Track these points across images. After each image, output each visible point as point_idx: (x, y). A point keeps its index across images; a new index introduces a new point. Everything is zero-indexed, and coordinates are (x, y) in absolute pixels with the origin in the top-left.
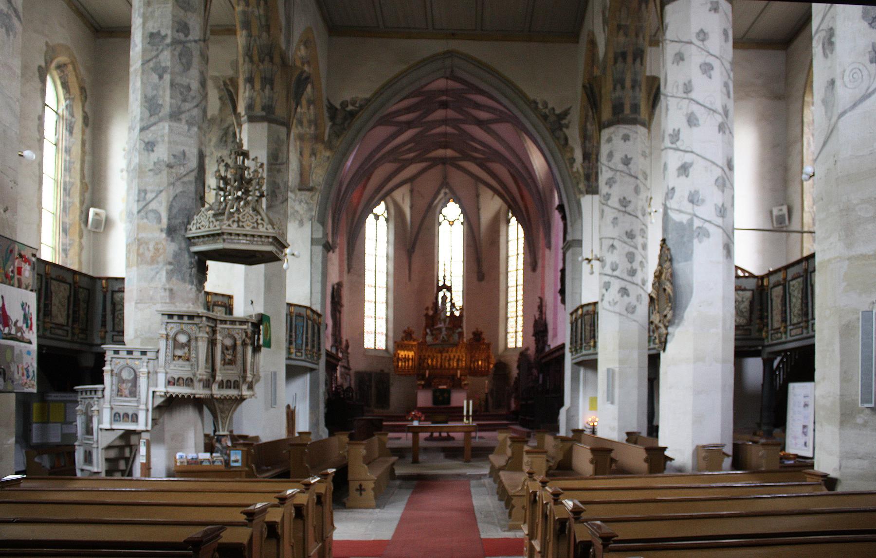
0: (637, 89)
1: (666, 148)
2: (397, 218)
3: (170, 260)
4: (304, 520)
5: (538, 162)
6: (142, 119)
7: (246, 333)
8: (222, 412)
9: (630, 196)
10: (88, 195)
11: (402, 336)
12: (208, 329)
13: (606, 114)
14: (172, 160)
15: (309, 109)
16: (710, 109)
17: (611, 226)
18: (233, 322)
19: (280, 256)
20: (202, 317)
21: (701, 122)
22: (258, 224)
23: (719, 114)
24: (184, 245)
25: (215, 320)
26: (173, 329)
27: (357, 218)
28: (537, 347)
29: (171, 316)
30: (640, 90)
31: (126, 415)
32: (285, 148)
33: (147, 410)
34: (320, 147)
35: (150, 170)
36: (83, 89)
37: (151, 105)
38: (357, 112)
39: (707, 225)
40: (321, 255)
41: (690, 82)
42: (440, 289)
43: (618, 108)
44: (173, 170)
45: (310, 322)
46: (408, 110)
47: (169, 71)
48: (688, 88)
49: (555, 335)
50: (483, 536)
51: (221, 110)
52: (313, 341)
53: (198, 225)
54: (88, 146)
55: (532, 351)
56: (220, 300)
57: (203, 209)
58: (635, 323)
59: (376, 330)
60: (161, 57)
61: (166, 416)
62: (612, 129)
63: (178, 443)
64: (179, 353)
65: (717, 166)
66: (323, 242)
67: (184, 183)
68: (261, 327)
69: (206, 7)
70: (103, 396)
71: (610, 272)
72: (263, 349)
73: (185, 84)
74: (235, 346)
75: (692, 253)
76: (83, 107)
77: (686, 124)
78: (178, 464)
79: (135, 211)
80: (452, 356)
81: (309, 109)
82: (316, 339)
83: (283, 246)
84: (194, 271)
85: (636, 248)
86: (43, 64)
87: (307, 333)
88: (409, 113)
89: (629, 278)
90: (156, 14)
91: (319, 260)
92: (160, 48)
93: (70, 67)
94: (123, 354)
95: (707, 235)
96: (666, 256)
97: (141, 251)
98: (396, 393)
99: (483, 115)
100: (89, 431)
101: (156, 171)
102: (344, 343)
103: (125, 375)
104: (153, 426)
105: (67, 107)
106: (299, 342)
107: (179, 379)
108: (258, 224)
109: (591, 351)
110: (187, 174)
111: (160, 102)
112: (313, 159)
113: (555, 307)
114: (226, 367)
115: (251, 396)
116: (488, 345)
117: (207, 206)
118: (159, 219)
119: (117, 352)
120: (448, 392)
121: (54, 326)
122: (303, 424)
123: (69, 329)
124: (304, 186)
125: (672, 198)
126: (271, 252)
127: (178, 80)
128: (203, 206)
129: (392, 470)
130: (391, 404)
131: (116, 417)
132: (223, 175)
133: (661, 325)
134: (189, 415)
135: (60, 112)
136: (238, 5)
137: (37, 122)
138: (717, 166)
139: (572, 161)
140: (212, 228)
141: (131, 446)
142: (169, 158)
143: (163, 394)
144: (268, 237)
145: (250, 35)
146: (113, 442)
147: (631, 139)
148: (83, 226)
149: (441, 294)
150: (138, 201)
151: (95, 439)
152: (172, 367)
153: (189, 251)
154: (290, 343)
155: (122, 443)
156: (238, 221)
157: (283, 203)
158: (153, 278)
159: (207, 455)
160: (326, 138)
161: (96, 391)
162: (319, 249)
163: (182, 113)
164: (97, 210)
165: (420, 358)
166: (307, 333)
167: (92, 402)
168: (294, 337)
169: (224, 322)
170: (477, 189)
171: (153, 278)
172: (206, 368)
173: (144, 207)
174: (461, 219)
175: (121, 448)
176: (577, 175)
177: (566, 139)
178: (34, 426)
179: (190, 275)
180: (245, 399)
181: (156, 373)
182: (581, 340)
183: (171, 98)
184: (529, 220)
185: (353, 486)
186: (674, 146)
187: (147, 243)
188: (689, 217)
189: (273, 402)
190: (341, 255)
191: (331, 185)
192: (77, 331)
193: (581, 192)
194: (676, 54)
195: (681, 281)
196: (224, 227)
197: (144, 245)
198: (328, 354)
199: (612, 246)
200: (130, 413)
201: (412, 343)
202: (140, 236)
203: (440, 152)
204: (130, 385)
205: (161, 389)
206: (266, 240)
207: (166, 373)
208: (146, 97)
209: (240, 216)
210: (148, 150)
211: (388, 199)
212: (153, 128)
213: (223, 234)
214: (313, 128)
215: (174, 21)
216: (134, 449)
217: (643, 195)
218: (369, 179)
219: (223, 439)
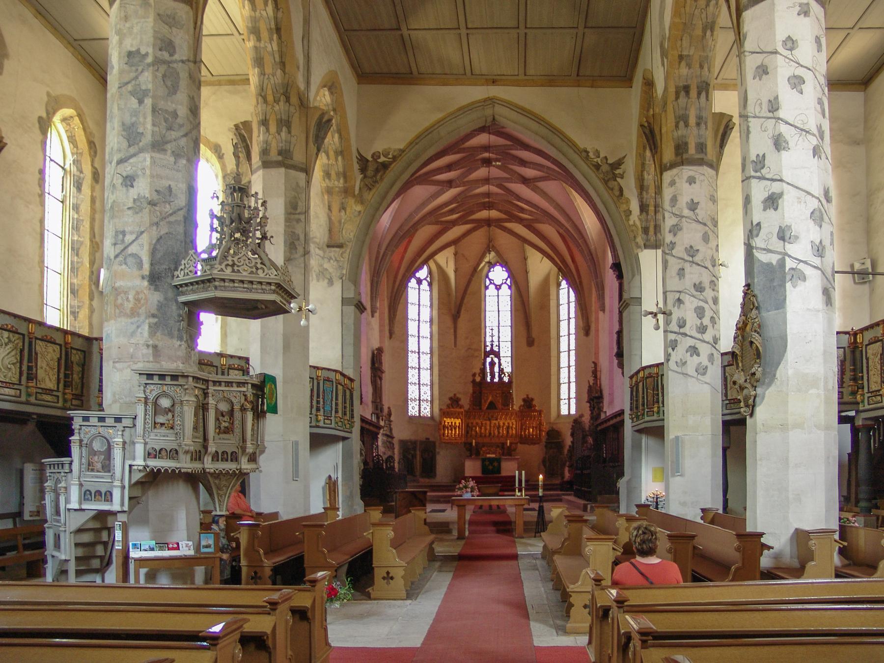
0: (703, 126)
1: (750, 177)
2: (439, 280)
3: (154, 311)
4: (270, 653)
5: (589, 221)
7: (245, 396)
8: (219, 488)
9: (699, 245)
11: (450, 404)
13: (668, 154)
14: (155, 197)
15: (337, 160)
16: (802, 130)
17: (677, 278)
20: (187, 376)
21: (791, 144)
22: (257, 269)
23: (814, 135)
24: (170, 294)
25: (207, 381)
26: (153, 391)
27: (397, 283)
28: (592, 413)
29: (150, 376)
30: (706, 128)
31: (99, 493)
33: (123, 487)
34: (351, 201)
35: (129, 208)
37: (131, 134)
38: (391, 163)
39: (801, 266)
40: (353, 317)
41: (776, 98)
42: (487, 354)
43: (680, 148)
44: (157, 208)
46: (449, 167)
47: (151, 94)
48: (774, 106)
49: (611, 402)
50: (537, 642)
55: (586, 419)
56: (236, 362)
58: (706, 385)
59: (420, 394)
60: (142, 79)
61: (151, 493)
62: (675, 171)
64: (161, 419)
65: (813, 196)
67: (170, 223)
69: (196, 23)
70: (71, 471)
71: (676, 329)
72: (268, 415)
73: (171, 109)
74: (231, 413)
75: (785, 299)
77: (772, 147)
80: (501, 424)
81: (337, 160)
84: (183, 324)
85: (707, 302)
86: (44, 115)
87: (337, 399)
88: (450, 171)
89: (699, 336)
90: (135, 30)
91: (350, 321)
92: (140, 69)
94: (94, 421)
95: (803, 278)
96: (750, 302)
98: (443, 463)
99: (530, 173)
100: (58, 513)
102: (386, 410)
103: (97, 446)
104: (131, 508)
105: (74, 161)
106: (328, 408)
108: (257, 269)
109: (655, 417)
110: (174, 213)
111: (140, 130)
112: (343, 213)
113: (611, 371)
114: (222, 436)
115: (254, 470)
116: (540, 412)
118: (140, 265)
119: (86, 419)
120: (499, 461)
121: (40, 391)
123: (60, 394)
125: (757, 235)
126: (274, 302)
127: (162, 104)
129: (431, 550)
130: (437, 473)
131: (87, 495)
133: (748, 386)
135: (67, 167)
136: (249, 40)
137: (38, 176)
138: (813, 196)
139: (629, 213)
142: (151, 195)
143: (141, 468)
144: (270, 284)
145: (262, 74)
146: (83, 525)
147: (697, 181)
148: (93, 287)
149: (489, 360)
151: (63, 521)
154: (318, 410)
156: (233, 265)
160: (357, 192)
162: (351, 309)
163: (167, 143)
165: (467, 426)
166: (337, 399)
168: (322, 403)
170: (524, 251)
171: (133, 334)
172: (194, 437)
174: (508, 282)
175: (97, 531)
176: (634, 228)
177: (621, 190)
179: (179, 330)
181: (134, 443)
182: (643, 405)
183: (154, 125)
184: (581, 282)
185: (379, 573)
186: (758, 174)
187: (126, 293)
188: (780, 257)
190: (381, 319)
191: (364, 242)
192: (69, 397)
193: (638, 247)
194: (758, 68)
195: (771, 331)
196: (215, 272)
199: (679, 300)
200: (103, 491)
201: (458, 410)
203: (484, 214)
205: (139, 462)
206: (268, 288)
207: (146, 444)
208: (123, 124)
209: (235, 259)
210: (126, 186)
211: (431, 263)
212: (131, 161)
213: (214, 279)
214: (342, 181)
215: (155, 38)
216: (110, 530)
217: (712, 244)
218: (410, 241)
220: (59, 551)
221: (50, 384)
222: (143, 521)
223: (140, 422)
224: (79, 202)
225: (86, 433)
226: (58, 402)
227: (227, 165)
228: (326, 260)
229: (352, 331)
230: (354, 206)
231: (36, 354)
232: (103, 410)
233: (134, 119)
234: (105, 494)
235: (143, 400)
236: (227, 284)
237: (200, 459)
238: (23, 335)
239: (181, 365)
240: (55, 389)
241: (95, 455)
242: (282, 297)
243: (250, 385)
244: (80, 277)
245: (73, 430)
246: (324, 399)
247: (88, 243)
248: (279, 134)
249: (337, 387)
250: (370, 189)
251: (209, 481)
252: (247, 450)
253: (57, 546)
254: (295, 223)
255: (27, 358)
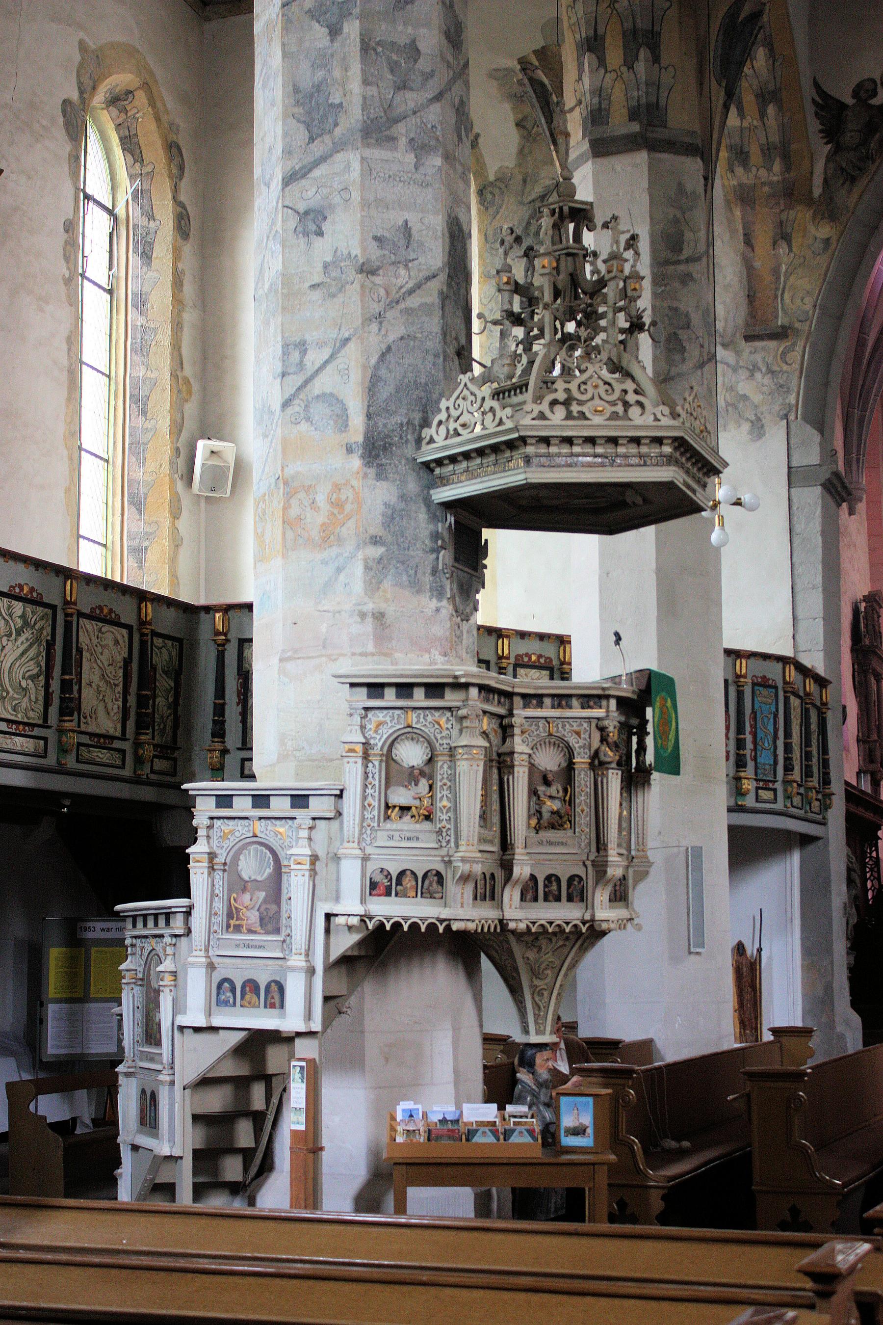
3: (375, 529)
6: (288, 152)
7: (602, 729)
8: (535, 973)
10: (191, 408)
12: (485, 724)
14: (375, 253)
15: (763, 115)
18: (562, 700)
19: (699, 497)
20: (466, 686)
22: (626, 405)
24: (413, 486)
29: (375, 689)
31: (251, 986)
32: (699, 215)
33: (311, 971)
34: (801, 215)
35: (313, 287)
36: (173, 149)
37: (313, 111)
44: (378, 280)
45: (795, 702)
51: (521, 152)
52: (808, 756)
53: (452, 425)
54: (189, 289)
56: (533, 648)
57: (464, 378)
61: (368, 987)
63: (402, 1073)
66: (825, 474)
67: (408, 311)
68: (649, 711)
70: (189, 931)
72: (655, 776)
73: (403, 40)
74: (569, 768)
76: (175, 190)
78: (400, 1139)
79: (277, 405)
81: (763, 115)
82: (814, 749)
83: (707, 468)
84: (446, 557)
86: (75, 96)
87: (788, 734)
93: (141, 97)
94: (243, 806)
97: (294, 511)
100: (152, 1035)
101: (329, 285)
103: (251, 867)
104: (327, 1022)
106: (765, 758)
107: (402, 873)
108: (626, 405)
110: (419, 286)
111: (336, 99)
115: (622, 924)
117: (477, 370)
118: (342, 420)
119: (224, 801)
121: (85, 739)
122: (784, 1004)
123: (126, 746)
124: (760, 329)
126: (670, 486)
127: (382, 31)
128: (466, 368)
131: (225, 991)
132: (521, 281)
134: (433, 984)
135: (120, 210)
137: (62, 237)
140: (492, 428)
141: (268, 1079)
142: (364, 250)
143: (355, 921)
144: (658, 441)
146: (213, 1067)
148: (180, 486)
150: (283, 375)
152: (382, 839)
153: (427, 501)
154: (740, 763)
155: (242, 1070)
156: (567, 403)
157: (702, 366)
158: (328, 586)
159: (490, 1112)
160: (817, 191)
161: (168, 916)
162: (812, 496)
163: (396, 121)
164: (215, 444)
166: (788, 734)
167: (159, 948)
168: (749, 745)
169: (533, 699)
171: (328, 586)
172: (482, 840)
173: (300, 389)
175: (241, 1084)
178: (52, 1008)
179: (434, 572)
180: (604, 933)
181: (336, 858)
183: (366, 82)
187: (308, 489)
189: (694, 939)
192: (148, 751)
196: (527, 421)
197: (302, 495)
198: (852, 795)
202: (290, 471)
204: (262, 895)
205: (351, 904)
206: (655, 450)
207: (365, 859)
208: (296, 90)
209: (573, 386)
210: (306, 234)
212: (316, 173)
213: (523, 440)
214: (777, 167)
216: (274, 1085)
219: (540, 1059)
220: (156, 1136)
221: (108, 724)
222: (351, 1060)
223: (351, 804)
224: (146, 288)
225: (224, 837)
226: (123, 767)
227: (488, 160)
228: (743, 374)
229: (819, 551)
230: (812, 229)
231: (80, 651)
232: (252, 777)
233: (320, 74)
234: (268, 988)
235: (359, 748)
236: (553, 449)
237: (493, 898)
238: (53, 608)
239: (440, 659)
240: (118, 734)
241: (244, 890)
242: (687, 472)
243: (613, 703)
244: (151, 466)
245: (195, 830)
246: (754, 735)
247: (167, 380)
248: (631, 67)
249: (787, 700)
250: (853, 179)
251: (510, 952)
252: (610, 872)
253: (149, 1117)
254: (677, 285)
255: (61, 661)
